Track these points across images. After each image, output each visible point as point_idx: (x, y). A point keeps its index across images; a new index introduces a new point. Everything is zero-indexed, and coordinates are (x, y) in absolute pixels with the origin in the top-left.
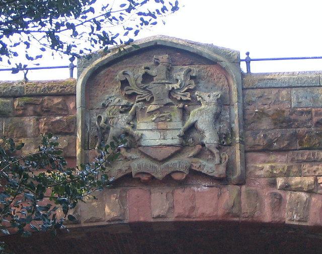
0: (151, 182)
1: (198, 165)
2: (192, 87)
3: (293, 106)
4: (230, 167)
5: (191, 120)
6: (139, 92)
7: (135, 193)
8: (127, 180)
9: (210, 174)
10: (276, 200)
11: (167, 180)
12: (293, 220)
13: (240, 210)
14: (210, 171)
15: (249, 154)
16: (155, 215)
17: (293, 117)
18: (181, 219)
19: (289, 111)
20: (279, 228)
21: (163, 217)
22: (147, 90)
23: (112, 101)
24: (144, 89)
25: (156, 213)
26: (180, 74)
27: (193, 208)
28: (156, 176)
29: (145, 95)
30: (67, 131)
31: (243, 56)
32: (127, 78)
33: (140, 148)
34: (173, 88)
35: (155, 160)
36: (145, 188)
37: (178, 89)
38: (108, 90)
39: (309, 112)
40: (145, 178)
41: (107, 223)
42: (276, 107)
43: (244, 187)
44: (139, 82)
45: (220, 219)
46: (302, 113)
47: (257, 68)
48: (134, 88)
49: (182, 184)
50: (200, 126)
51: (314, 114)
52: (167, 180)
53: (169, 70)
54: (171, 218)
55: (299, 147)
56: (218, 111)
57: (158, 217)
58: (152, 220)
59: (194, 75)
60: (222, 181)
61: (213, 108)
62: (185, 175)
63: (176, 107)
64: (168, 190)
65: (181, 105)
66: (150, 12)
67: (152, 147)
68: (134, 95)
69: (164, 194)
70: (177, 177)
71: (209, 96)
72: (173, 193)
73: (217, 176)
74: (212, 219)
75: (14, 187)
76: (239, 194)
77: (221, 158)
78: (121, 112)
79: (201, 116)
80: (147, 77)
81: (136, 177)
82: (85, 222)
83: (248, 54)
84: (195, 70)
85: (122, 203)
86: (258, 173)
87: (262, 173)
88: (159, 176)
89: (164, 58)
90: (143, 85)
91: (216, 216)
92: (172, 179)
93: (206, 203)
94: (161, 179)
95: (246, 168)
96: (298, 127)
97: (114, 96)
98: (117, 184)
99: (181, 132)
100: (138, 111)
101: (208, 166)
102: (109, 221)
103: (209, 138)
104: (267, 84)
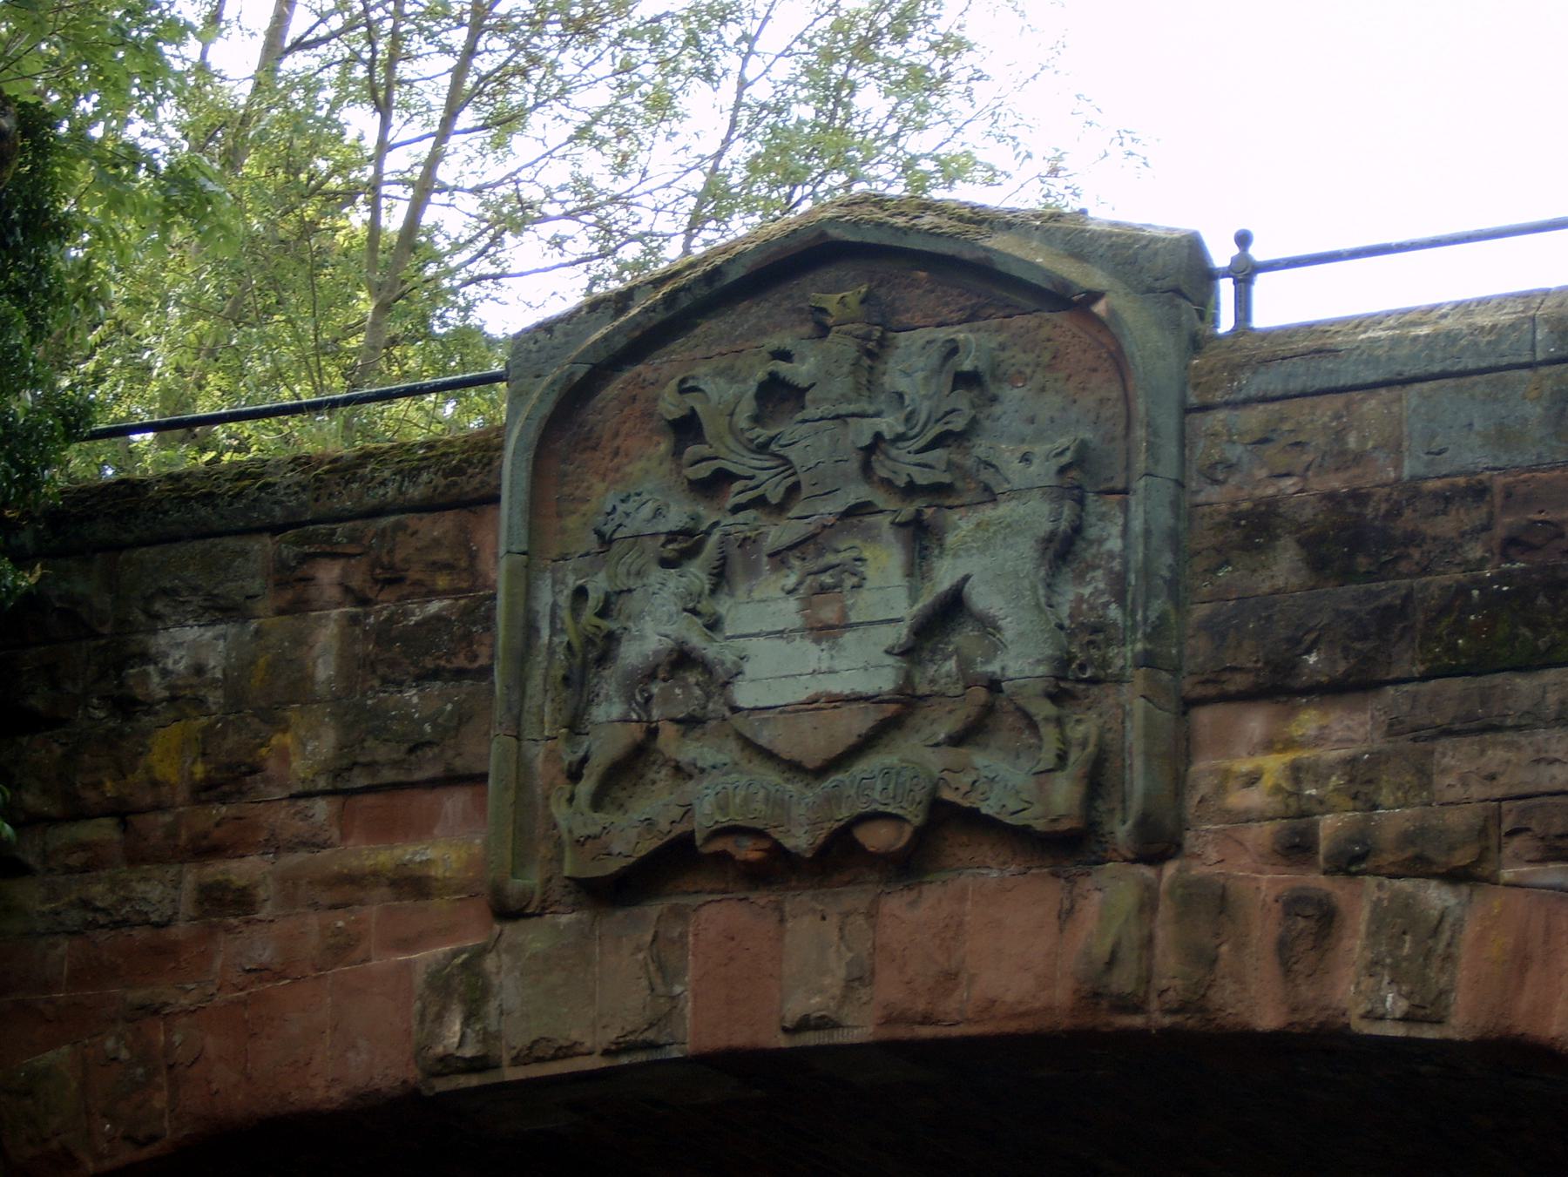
0: (774, 869)
1: (966, 780)
2: (958, 424)
3: (1406, 474)
4: (1099, 778)
5: (945, 575)
6: (741, 462)
7: (715, 917)
8: (674, 863)
9: (1009, 820)
10: (1302, 923)
11: (839, 857)
12: (1382, 1018)
13: (1147, 979)
14: (1013, 805)
15: (1204, 717)
16: (789, 1016)
17: (1409, 520)
18: (902, 1032)
19: (165, 513)
20: (1322, 1049)
21: (824, 1023)
22: (775, 455)
23: (628, 515)
24: (762, 448)
25: (799, 1004)
26: (910, 368)
27: (949, 979)
28: (789, 843)
29: (763, 476)
30: (460, 661)
31: (1221, 254)
32: (698, 408)
33: (738, 721)
34: (878, 436)
35: (794, 768)
36: (761, 898)
37: (901, 437)
38: (629, 469)
39: (1479, 492)
40: (748, 851)
41: (603, 1063)
42: (1337, 483)
43: (1170, 869)
44: (742, 422)
45: (1066, 1023)
46: (1446, 499)
47: (1279, 305)
48: (723, 452)
49: (910, 865)
50: (982, 598)
51: (1498, 500)
52: (839, 857)
53: (874, 352)
54: (860, 1028)
55: (1418, 669)
56: (1064, 526)
57: (804, 1025)
58: (783, 1042)
59: (967, 366)
60: (1067, 848)
61: (1037, 515)
62: (908, 831)
63: (884, 521)
64: (855, 898)
65: (908, 511)
66: (751, 84)
67: (782, 709)
68: (722, 479)
69: (833, 920)
70: (877, 838)
71: (1026, 458)
72: (871, 915)
73: (1040, 826)
74: (1028, 1025)
75: (1352, 860)
76: (1148, 904)
77: (1064, 740)
78: (666, 563)
79: (990, 559)
80: (777, 395)
81: (718, 845)
82: (517, 1061)
83: (1243, 239)
84: (977, 344)
85: (661, 968)
86: (1240, 799)
87: (1254, 798)
88: (800, 840)
89: (841, 296)
90: (758, 430)
91: (1049, 1009)
92: (856, 849)
93: (1004, 954)
94: (809, 855)
95: (1180, 784)
96: (1425, 570)
97: (642, 490)
98: (616, 891)
99: (899, 634)
100: (734, 552)
101: (1004, 780)
102: (606, 1053)
103: (1021, 660)
104: (1320, 364)
